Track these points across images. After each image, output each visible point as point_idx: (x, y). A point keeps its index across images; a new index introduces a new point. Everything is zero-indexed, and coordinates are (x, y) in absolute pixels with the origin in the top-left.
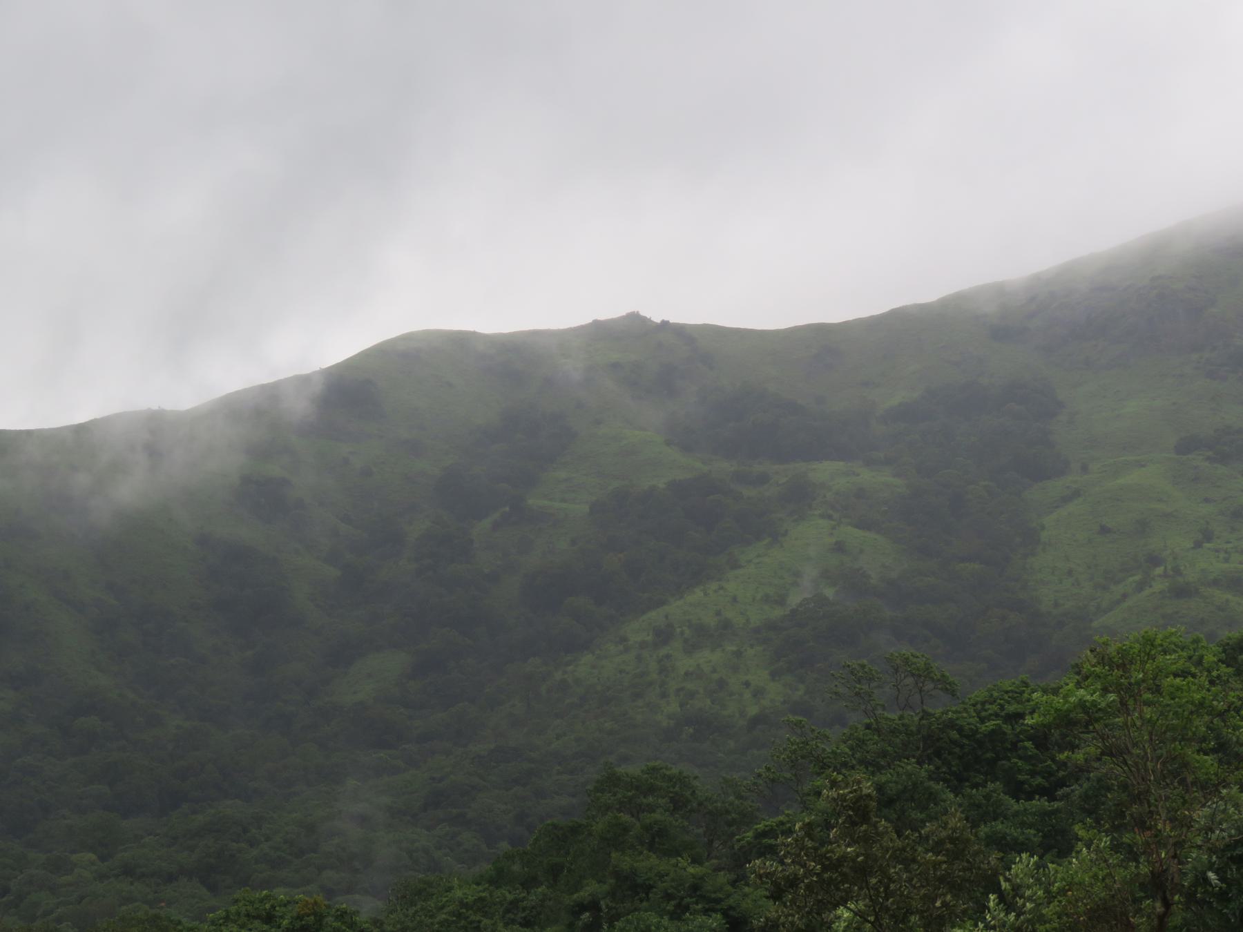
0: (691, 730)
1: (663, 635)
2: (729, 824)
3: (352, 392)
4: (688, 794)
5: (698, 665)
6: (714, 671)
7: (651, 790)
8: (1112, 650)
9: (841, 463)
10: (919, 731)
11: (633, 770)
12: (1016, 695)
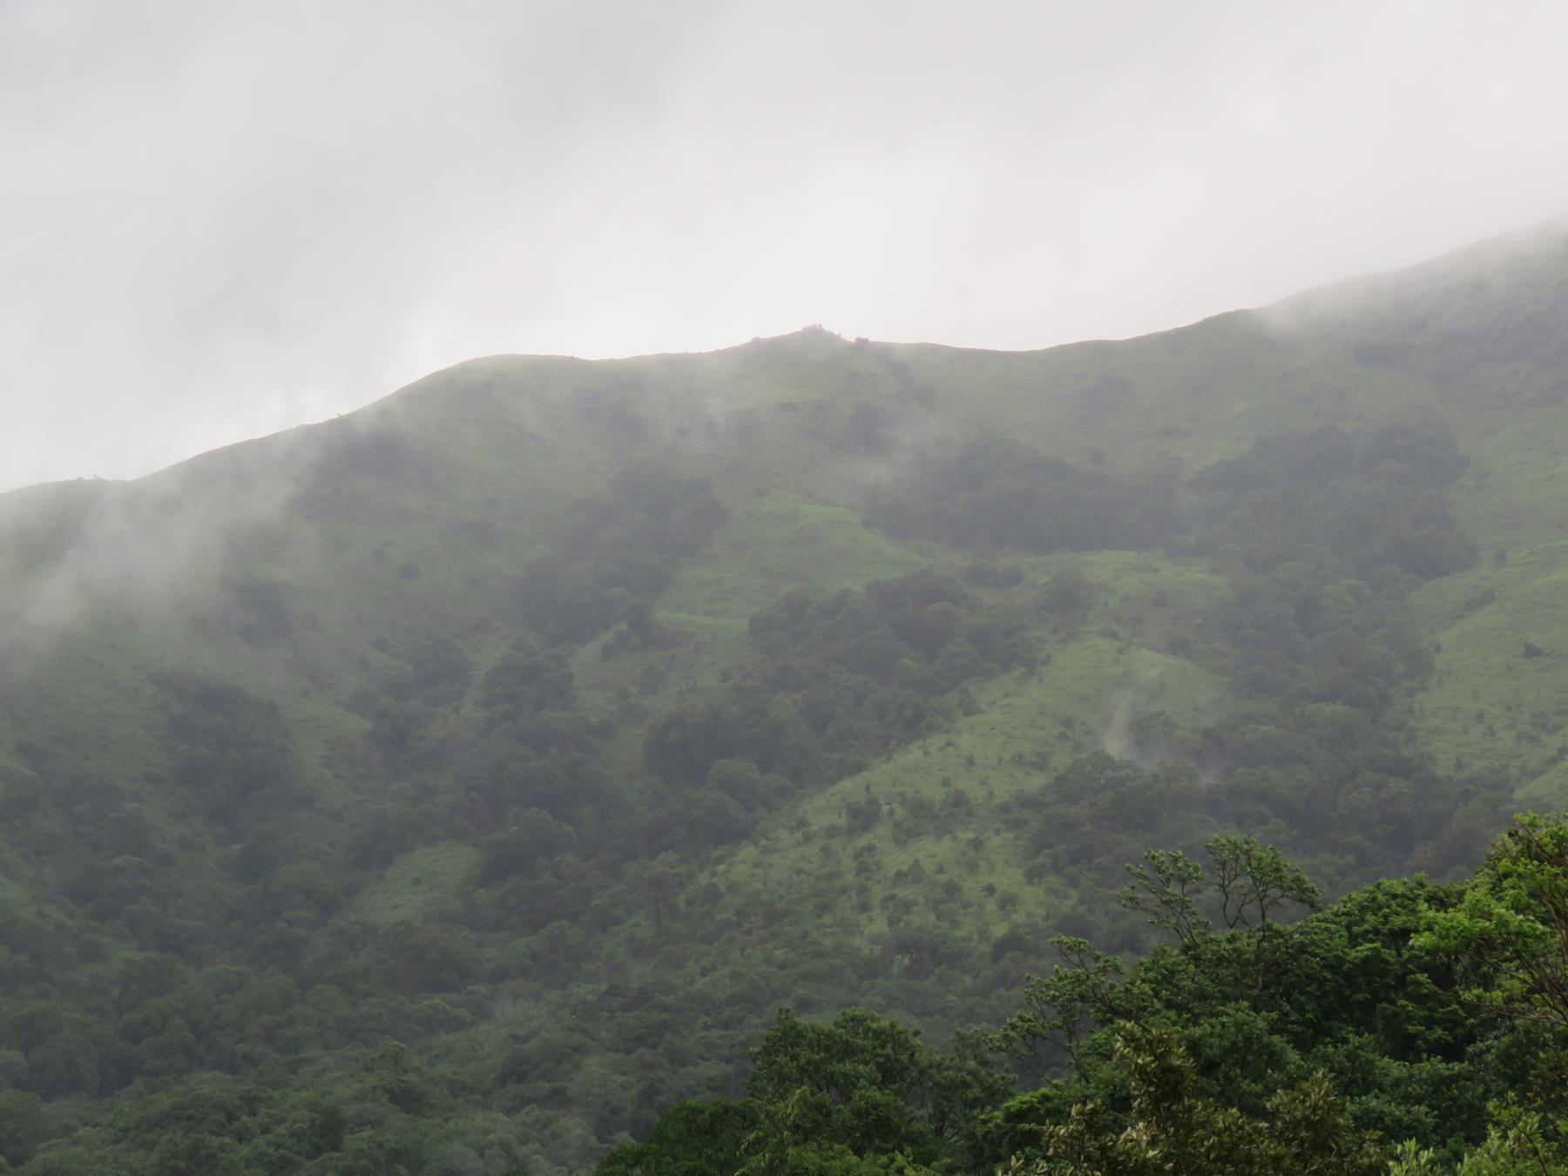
0: (907, 961)
1: (863, 817)
2: (971, 1105)
3: (360, 466)
4: (904, 1058)
5: (916, 861)
6: (941, 870)
7: (848, 1051)
8: (1541, 835)
9: (1132, 554)
10: (1258, 959)
11: (823, 1020)
12: (1406, 901)
